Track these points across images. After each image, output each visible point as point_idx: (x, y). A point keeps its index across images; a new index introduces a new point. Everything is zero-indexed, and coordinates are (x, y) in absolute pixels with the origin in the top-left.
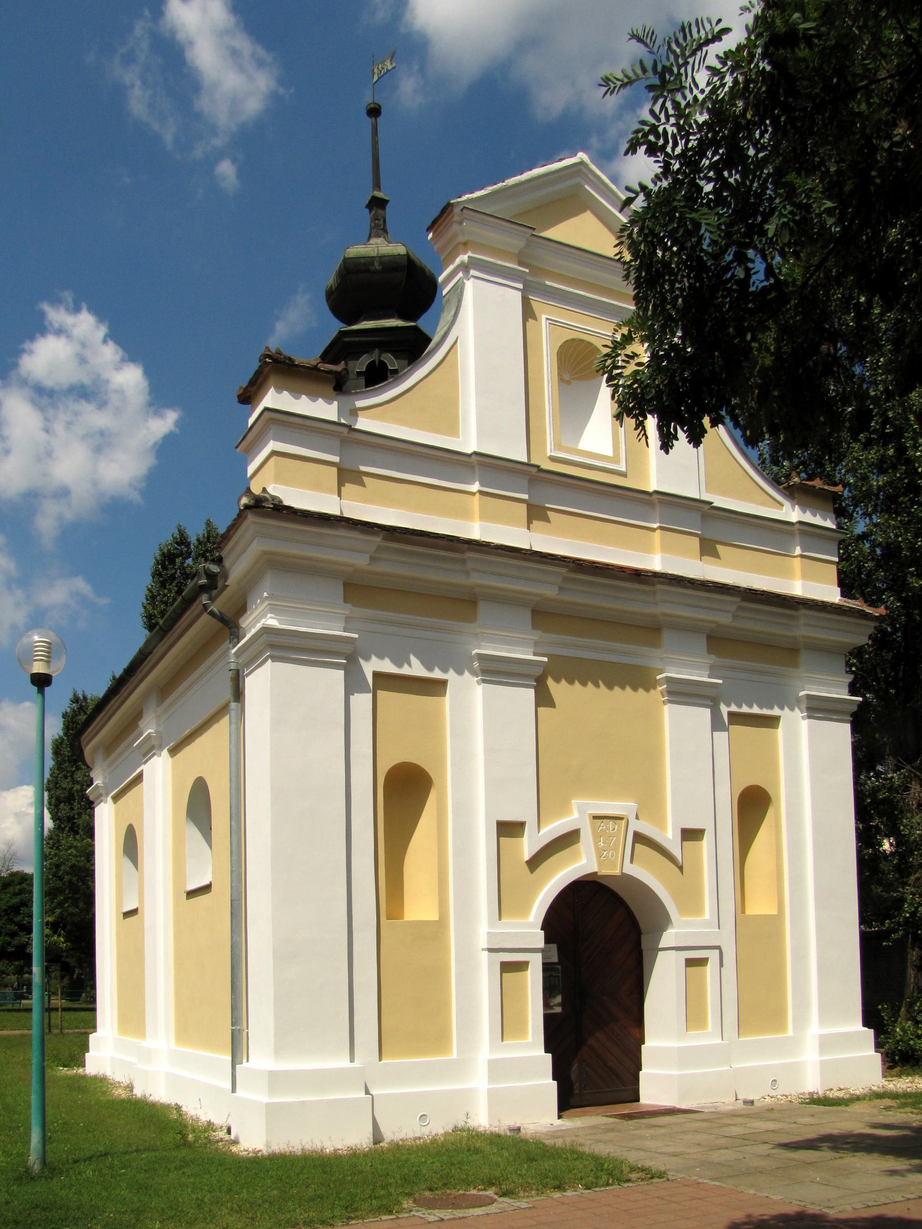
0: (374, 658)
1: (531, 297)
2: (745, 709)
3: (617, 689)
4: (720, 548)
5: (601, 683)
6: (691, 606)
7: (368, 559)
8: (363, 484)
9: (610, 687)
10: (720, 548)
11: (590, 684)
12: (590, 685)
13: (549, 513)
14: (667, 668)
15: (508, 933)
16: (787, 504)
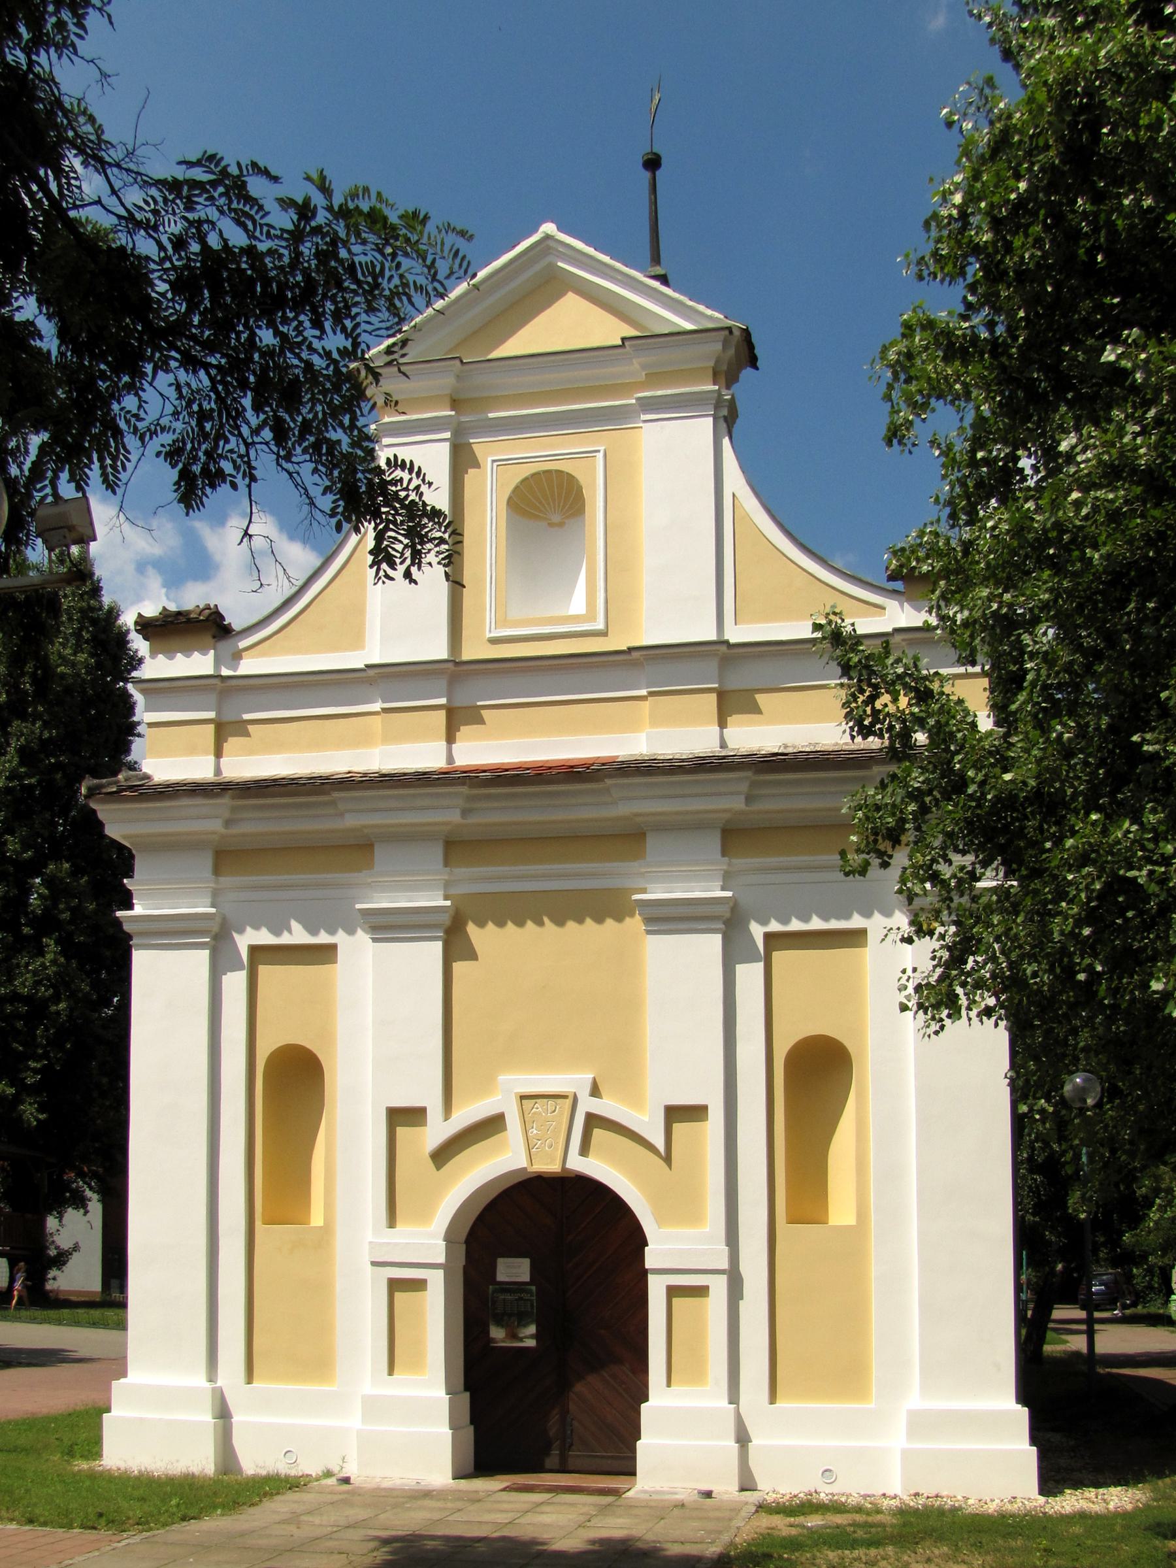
0: (249, 929)
1: (471, 441)
2: (796, 925)
3: (571, 925)
4: (761, 698)
5: (546, 920)
6: (670, 797)
7: (743, 800)
8: (248, 735)
9: (560, 922)
10: (761, 698)
11: (530, 924)
12: (490, 926)
13: (483, 712)
14: (649, 886)
15: (396, 1244)
16: (892, 605)
